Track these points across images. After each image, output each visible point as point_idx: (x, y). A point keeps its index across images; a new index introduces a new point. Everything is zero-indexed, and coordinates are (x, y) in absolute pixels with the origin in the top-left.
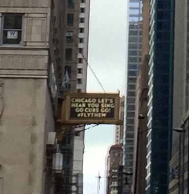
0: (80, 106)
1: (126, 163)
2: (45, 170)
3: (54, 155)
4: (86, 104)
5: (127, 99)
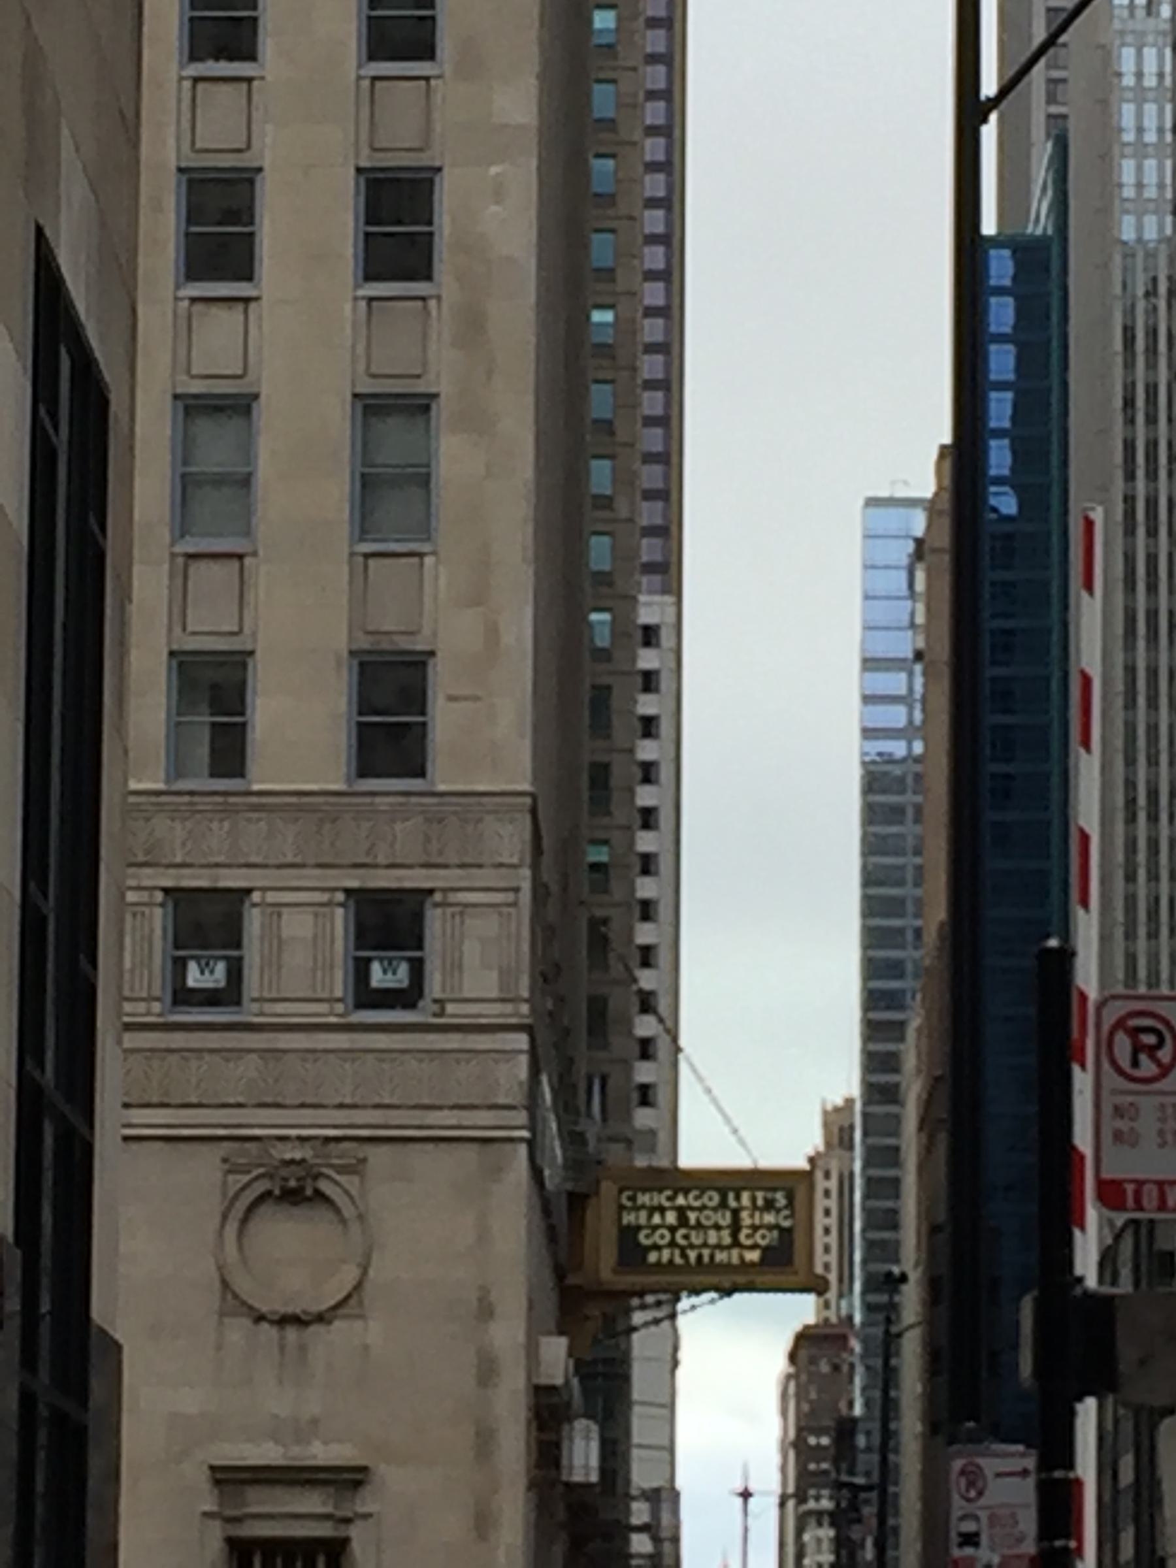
0: (657, 1219)
1: (867, 1404)
2: (533, 1485)
3: (566, 1427)
4: (681, 1212)
5: (865, 1116)
